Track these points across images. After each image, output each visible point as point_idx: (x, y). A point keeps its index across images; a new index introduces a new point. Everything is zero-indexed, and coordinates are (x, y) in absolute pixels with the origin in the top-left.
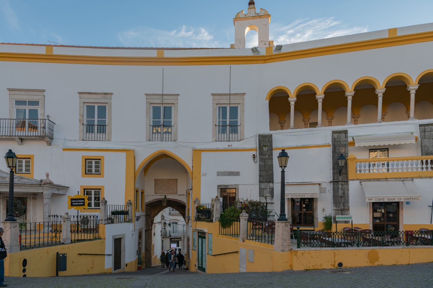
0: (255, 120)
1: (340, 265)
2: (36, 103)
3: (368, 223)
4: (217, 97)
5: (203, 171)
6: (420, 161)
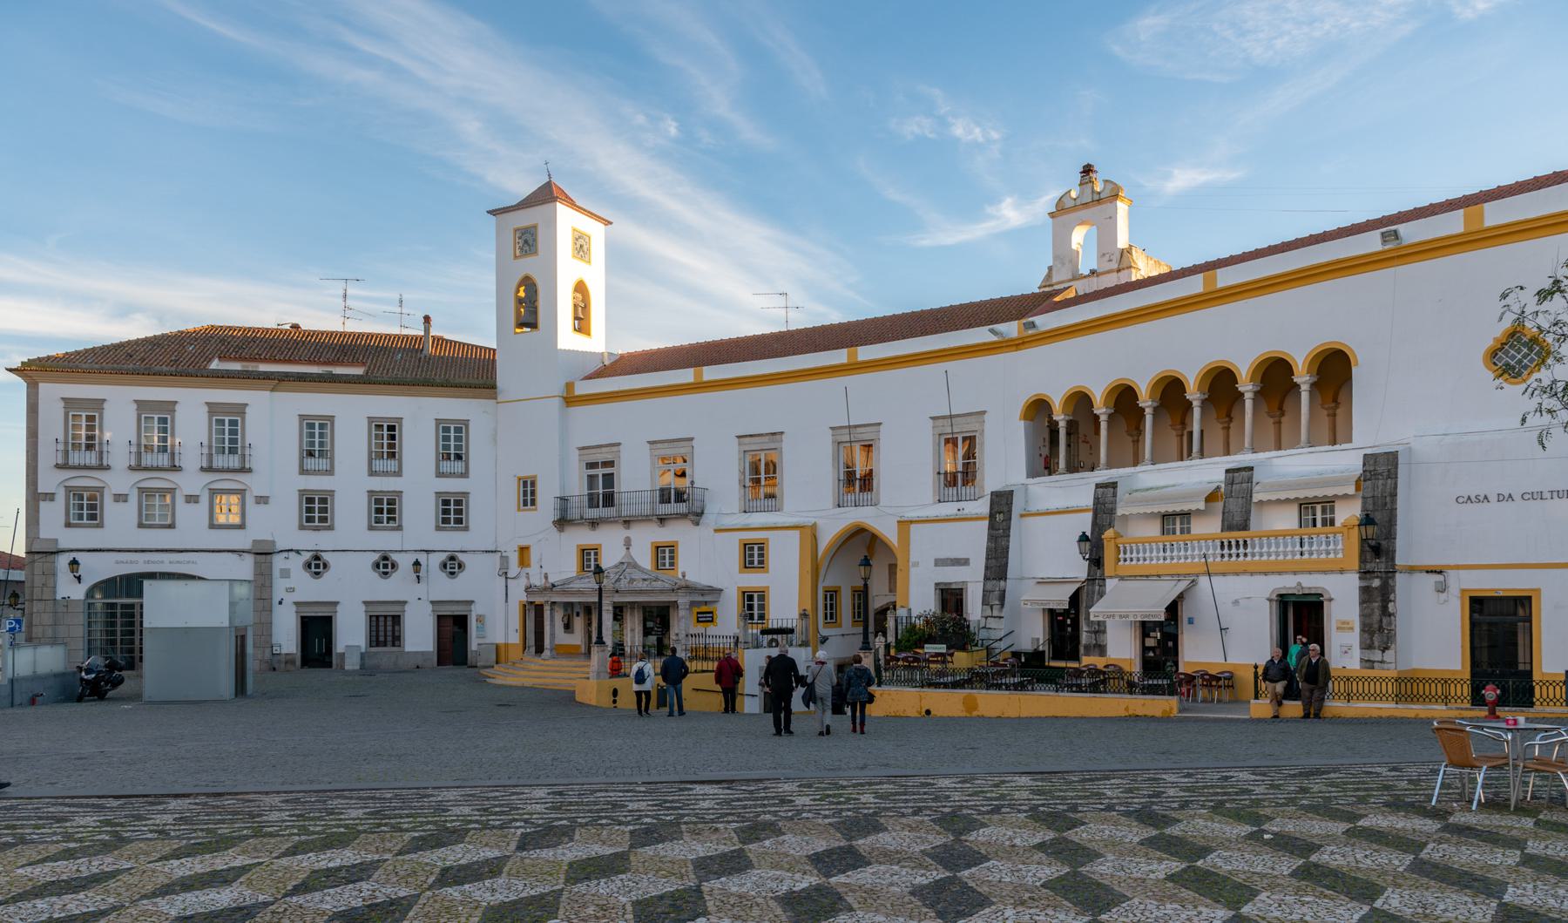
0: (1005, 459)
1: (928, 712)
2: (610, 464)
3: (1458, 667)
4: (940, 422)
5: (913, 559)
6: (1218, 543)
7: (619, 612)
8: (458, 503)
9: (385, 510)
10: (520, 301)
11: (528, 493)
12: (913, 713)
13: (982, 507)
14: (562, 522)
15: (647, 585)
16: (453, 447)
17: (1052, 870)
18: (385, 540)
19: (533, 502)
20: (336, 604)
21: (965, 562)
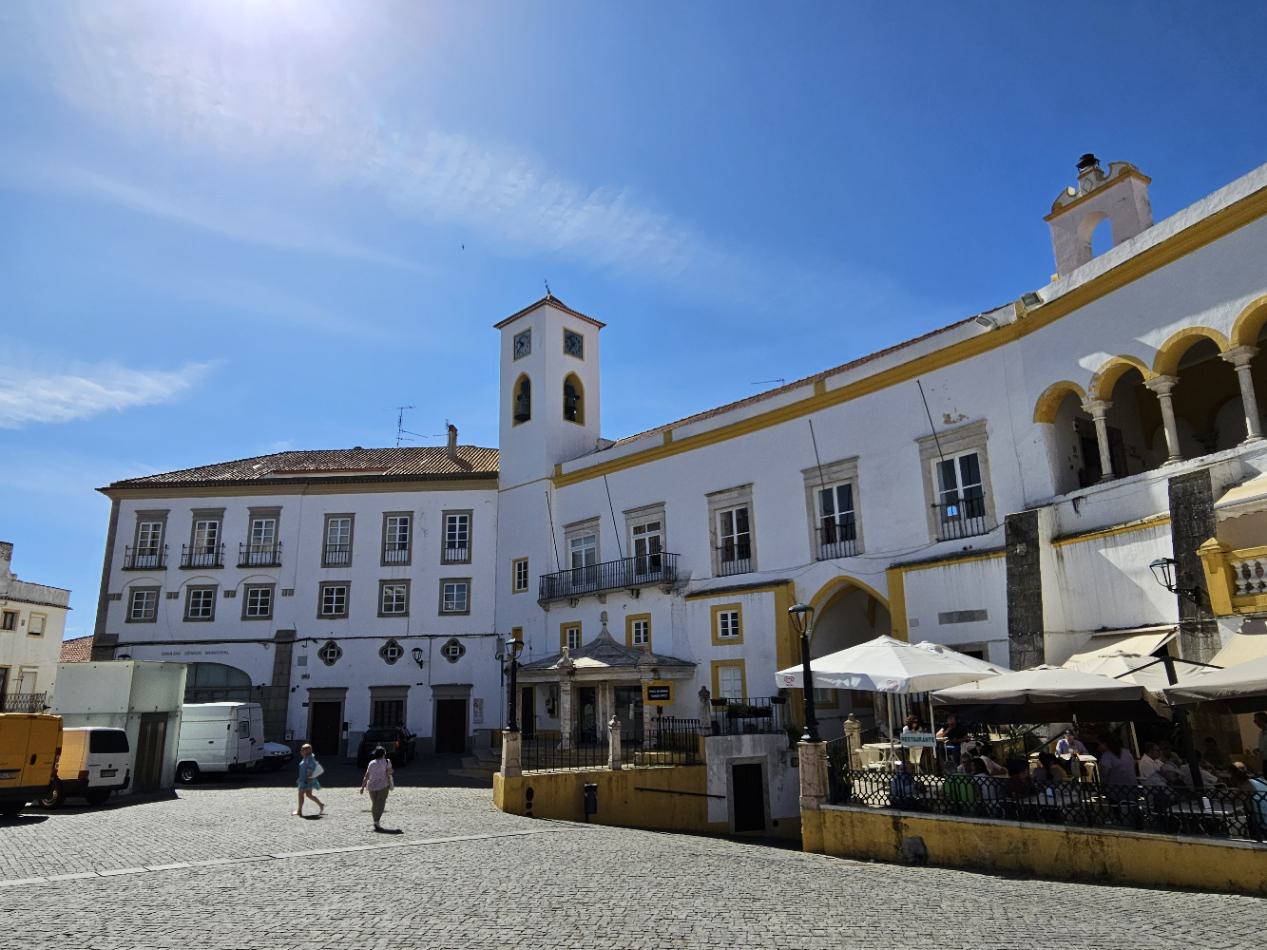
2: (655, 526)
9: (394, 603)
13: (998, 538)
16: (457, 533)
18: (394, 627)
19: (525, 585)
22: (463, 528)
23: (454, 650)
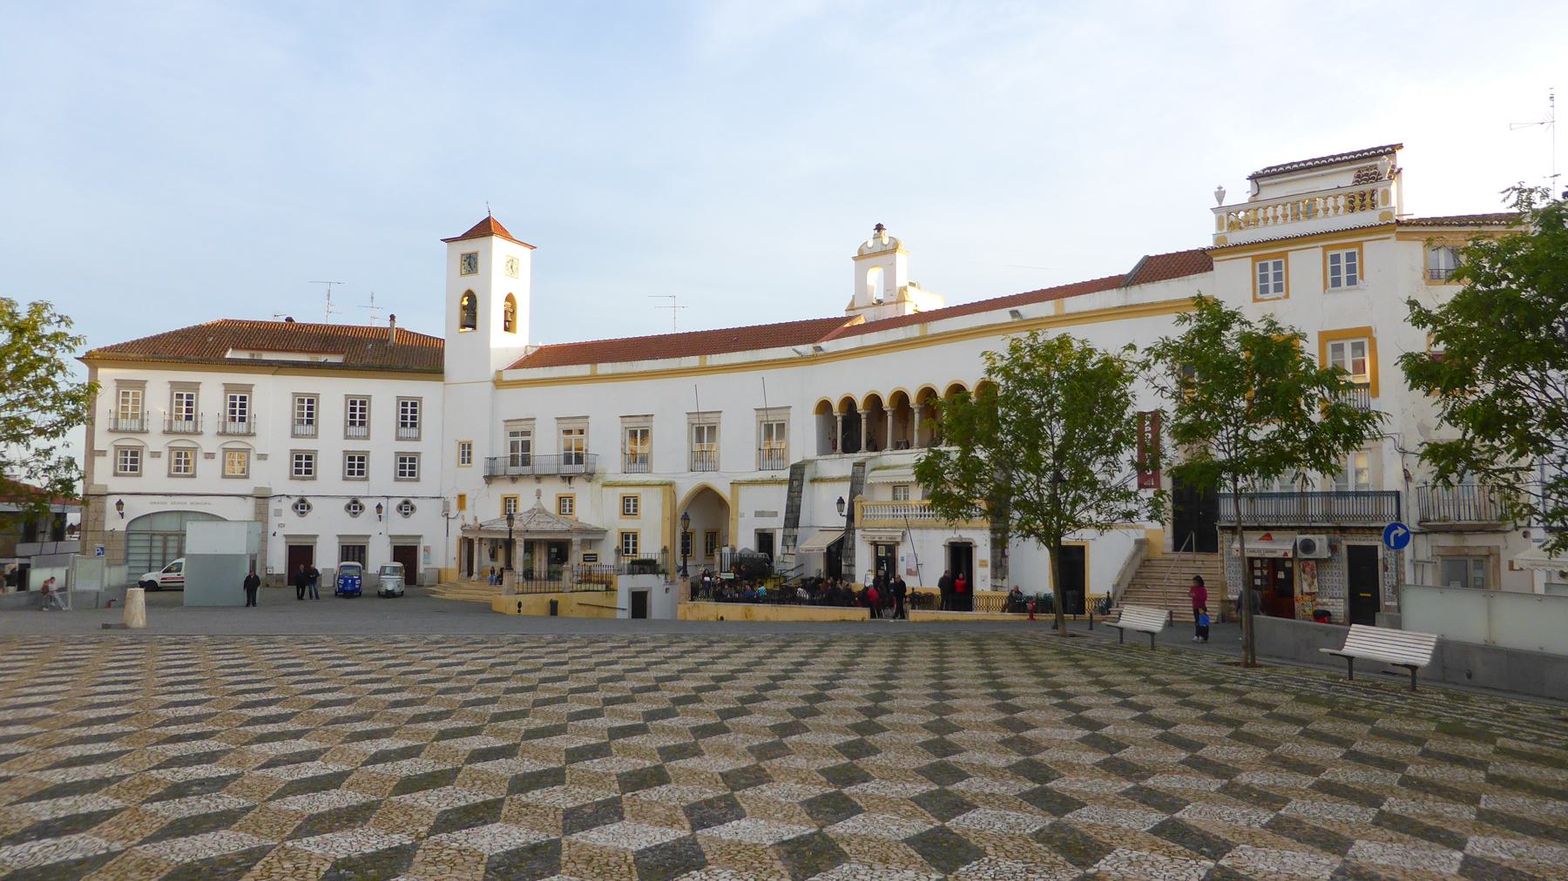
0: (803, 440)
2: (527, 433)
7: (530, 546)
8: (402, 474)
9: (356, 465)
10: (464, 308)
11: (466, 452)
12: (712, 619)
13: (786, 474)
14: (490, 478)
15: (554, 526)
16: (409, 415)
17: (1038, 821)
18: (356, 488)
20: (316, 536)
21: (775, 514)
22: (413, 411)
23: (406, 508)
